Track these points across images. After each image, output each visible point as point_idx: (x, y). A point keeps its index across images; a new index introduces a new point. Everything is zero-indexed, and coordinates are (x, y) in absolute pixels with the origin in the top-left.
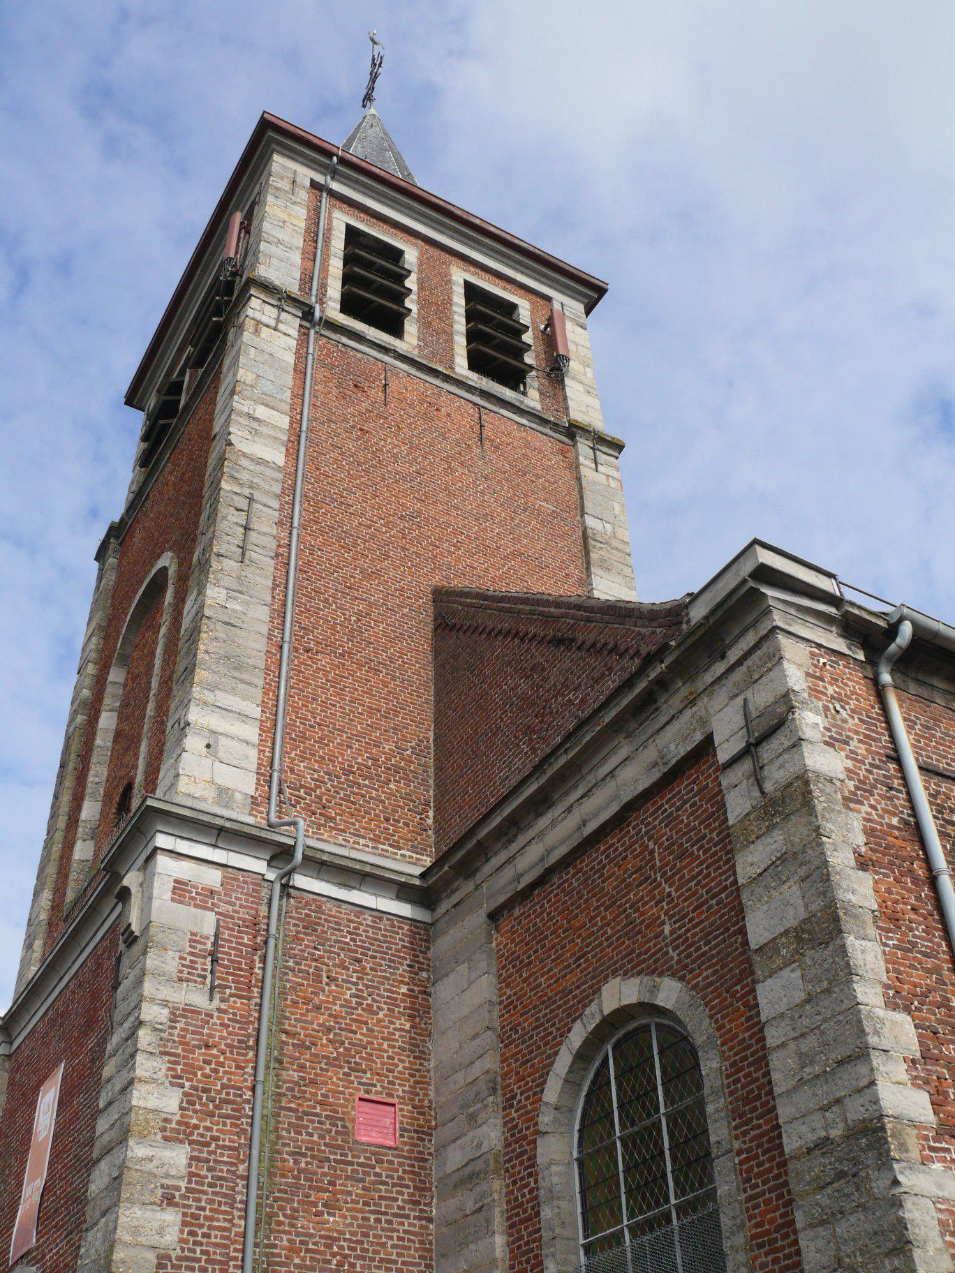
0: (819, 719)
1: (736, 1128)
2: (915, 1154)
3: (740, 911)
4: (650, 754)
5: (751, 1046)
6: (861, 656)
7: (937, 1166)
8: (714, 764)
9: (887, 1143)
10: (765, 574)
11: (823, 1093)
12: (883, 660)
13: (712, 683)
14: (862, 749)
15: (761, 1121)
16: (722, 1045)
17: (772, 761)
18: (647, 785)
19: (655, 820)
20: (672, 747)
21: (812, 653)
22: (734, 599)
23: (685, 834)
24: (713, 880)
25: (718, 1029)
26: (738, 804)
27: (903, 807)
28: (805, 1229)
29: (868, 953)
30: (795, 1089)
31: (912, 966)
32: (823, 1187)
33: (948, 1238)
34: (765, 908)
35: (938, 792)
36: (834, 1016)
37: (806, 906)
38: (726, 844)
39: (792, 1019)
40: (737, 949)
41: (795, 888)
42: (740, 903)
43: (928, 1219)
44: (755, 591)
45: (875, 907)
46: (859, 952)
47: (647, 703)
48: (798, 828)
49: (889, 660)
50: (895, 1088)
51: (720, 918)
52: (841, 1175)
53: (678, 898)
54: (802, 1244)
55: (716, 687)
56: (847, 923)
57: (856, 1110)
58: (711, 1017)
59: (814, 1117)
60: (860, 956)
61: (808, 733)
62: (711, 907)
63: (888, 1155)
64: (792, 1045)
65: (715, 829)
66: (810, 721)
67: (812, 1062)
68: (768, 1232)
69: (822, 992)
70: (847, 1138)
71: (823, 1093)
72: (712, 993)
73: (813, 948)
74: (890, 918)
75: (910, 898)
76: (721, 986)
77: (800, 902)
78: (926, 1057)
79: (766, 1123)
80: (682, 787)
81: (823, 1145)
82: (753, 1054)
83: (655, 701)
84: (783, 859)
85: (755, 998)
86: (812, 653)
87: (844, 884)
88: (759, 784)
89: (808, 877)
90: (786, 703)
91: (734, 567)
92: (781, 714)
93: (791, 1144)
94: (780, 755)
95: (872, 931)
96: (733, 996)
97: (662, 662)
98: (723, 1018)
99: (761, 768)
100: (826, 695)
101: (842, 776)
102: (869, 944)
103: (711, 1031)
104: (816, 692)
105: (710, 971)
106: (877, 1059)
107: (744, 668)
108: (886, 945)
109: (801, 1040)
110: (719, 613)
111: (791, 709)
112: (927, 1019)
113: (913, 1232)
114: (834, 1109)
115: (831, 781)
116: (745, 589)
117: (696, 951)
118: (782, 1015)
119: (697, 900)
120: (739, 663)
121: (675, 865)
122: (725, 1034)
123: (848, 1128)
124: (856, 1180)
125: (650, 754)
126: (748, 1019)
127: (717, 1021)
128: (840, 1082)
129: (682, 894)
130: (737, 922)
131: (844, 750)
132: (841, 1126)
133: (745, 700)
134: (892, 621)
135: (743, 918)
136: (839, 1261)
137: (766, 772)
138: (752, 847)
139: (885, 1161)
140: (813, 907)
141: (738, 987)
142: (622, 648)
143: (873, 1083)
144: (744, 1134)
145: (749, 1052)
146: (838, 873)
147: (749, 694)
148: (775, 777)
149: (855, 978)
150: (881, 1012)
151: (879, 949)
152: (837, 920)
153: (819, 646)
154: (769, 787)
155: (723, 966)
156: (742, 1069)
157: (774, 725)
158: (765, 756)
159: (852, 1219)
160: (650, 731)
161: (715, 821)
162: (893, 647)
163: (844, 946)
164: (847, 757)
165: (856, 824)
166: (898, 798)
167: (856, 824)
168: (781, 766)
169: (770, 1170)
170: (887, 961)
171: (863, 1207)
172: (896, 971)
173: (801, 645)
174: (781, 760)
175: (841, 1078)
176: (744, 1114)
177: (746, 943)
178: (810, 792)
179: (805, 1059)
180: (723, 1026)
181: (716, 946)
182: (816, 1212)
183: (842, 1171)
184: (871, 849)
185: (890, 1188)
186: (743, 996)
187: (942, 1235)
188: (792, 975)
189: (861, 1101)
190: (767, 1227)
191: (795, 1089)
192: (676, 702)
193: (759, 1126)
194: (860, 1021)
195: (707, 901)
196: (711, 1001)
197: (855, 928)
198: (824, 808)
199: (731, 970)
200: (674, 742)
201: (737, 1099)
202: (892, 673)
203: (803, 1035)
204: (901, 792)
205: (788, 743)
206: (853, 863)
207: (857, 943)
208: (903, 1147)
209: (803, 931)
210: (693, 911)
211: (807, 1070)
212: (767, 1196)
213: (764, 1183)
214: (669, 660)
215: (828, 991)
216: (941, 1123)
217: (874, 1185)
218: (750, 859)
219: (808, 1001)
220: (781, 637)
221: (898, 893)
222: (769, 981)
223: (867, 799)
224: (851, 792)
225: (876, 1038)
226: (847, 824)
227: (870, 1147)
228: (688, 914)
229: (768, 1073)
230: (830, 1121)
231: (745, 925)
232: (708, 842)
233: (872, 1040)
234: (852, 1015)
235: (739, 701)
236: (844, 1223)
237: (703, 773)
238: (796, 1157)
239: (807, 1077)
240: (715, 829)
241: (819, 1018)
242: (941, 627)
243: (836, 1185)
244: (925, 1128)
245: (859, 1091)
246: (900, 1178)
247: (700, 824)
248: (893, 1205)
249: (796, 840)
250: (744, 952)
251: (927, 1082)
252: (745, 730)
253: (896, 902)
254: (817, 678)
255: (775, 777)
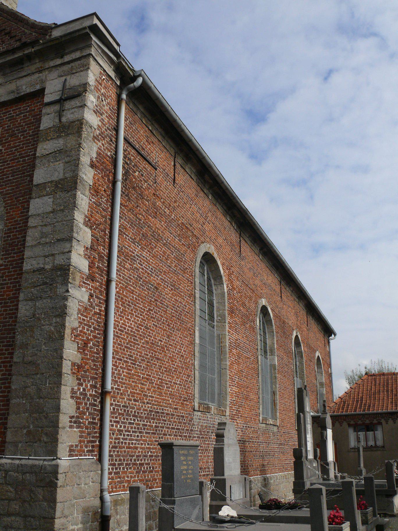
0: (94, 100)
1: (3, 255)
2: (77, 283)
3: (33, 167)
4: (12, 87)
5: (20, 224)
6: (118, 83)
7: (84, 289)
8: (40, 102)
9: (69, 275)
10: (94, 29)
11: (47, 250)
12: (126, 89)
13: (53, 67)
14: (106, 120)
15: (15, 255)
16: (7, 220)
17: (69, 109)
18: (5, 100)
19: (4, 116)
20: (24, 87)
21: (101, 72)
22: (77, 34)
23: (17, 127)
24: (23, 150)
25: (7, 213)
26: (47, 122)
27: (113, 150)
28: (23, 301)
29: (83, 201)
30: (35, 246)
31: (97, 212)
32: (36, 287)
33: (79, 316)
34: (46, 169)
35: (127, 150)
36: (62, 221)
37: (64, 173)
38: (37, 136)
39: (43, 217)
40: (26, 182)
41: (62, 165)
42: (35, 164)
43: (75, 307)
44: (88, 35)
45: (91, 184)
46: (80, 199)
47: (18, 64)
48: (71, 141)
49: (128, 90)
50: (78, 256)
51: (22, 167)
52: (45, 283)
53: (5, 153)
54: (20, 306)
55: (54, 69)
56: (80, 186)
57: (59, 260)
58: (5, 207)
59: (40, 259)
60: (80, 201)
61: (89, 104)
62: (20, 161)
63: (68, 280)
64: (40, 228)
65: (32, 129)
66: (91, 99)
67: (46, 237)
68: (5, 299)
69: (60, 210)
70: (52, 270)
71: (47, 250)
72: (8, 197)
73: (61, 192)
74: (95, 191)
75: (105, 186)
76: (14, 195)
77: (62, 171)
78: (92, 248)
79: (17, 256)
80: (22, 106)
81: (41, 270)
82: (19, 227)
83: (23, 64)
84: (60, 151)
85: (29, 205)
86: (101, 72)
87: (83, 170)
88: (60, 117)
89: (68, 162)
90: (84, 88)
91: (81, 21)
92: (80, 91)
93: (26, 267)
94: (74, 108)
95: (87, 193)
96: (18, 201)
97: (33, 48)
98: (10, 209)
99: (63, 111)
100: (100, 92)
101: (96, 127)
102: (85, 198)
103: (3, 213)
104: (97, 89)
105: (10, 188)
106: (74, 243)
107: (70, 66)
108: (91, 200)
109: (45, 227)
110: (68, 37)
111: (85, 91)
112: (96, 234)
113: (69, 311)
114: (50, 258)
115: (91, 127)
116: (84, 32)
117: (6, 178)
118: (39, 215)
119: (13, 157)
120: (69, 63)
121: (8, 139)
122: (10, 216)
123: (54, 266)
124: (51, 287)
125: (12, 87)
126: (21, 213)
127: (7, 210)
128: (56, 248)
129: (7, 152)
130: (29, 171)
131: (100, 117)
132: (51, 265)
133: (66, 80)
134: (135, 75)
135: (33, 171)
136: (34, 315)
137: (64, 113)
138: (47, 142)
139: (65, 282)
140: (67, 175)
141: (21, 198)
142: (13, 35)
143: (70, 251)
144: (6, 258)
145: (18, 226)
146: (82, 165)
147: (68, 78)
148: (68, 116)
149: (76, 209)
150: (81, 226)
151: (88, 201)
152: (76, 183)
153: (105, 71)
154: (64, 119)
155: (16, 188)
156: (13, 232)
157: (75, 94)
158: (67, 106)
159: (44, 301)
160: (16, 77)
161: (33, 126)
162: (132, 85)
163: (75, 195)
164: (100, 121)
165: (95, 148)
166: (112, 146)
167: (95, 148)
168: (72, 113)
169: (13, 275)
170: (89, 207)
171: (51, 297)
172: (91, 212)
173: (98, 67)
174: (73, 110)
175: (57, 246)
176: (8, 250)
177: (32, 181)
178: (82, 128)
179: (43, 235)
180: (9, 212)
181: (16, 179)
182: (30, 295)
183: (46, 282)
184: (97, 161)
185: (64, 293)
186: (23, 202)
187: (78, 314)
188: (49, 200)
189: (63, 257)
190: (5, 297)
191: (35, 246)
192: (33, 68)
193: (14, 257)
194: (72, 226)
195: (18, 158)
196: (7, 200)
197: (82, 189)
198: (85, 137)
199: (21, 190)
200: (26, 85)
201: (7, 244)
202: (127, 95)
203: (46, 225)
204: (114, 144)
205: (79, 104)
206: (89, 163)
207: (81, 195)
208: (74, 279)
209: (59, 183)
210: (10, 161)
211: (43, 239)
212: (9, 285)
213: (9, 280)
214: (36, 48)
215: (62, 211)
216: (90, 274)
217: (58, 290)
218: (45, 147)
219: (52, 212)
220: (91, 59)
221: (101, 182)
222: (37, 200)
223: (102, 141)
224: (97, 135)
225: (77, 235)
226: (91, 147)
227: (61, 275)
228: (8, 161)
229: (25, 237)
230: (47, 262)
231: (33, 174)
232: (27, 134)
233: (75, 235)
234: (70, 224)
235: (63, 79)
236: (40, 302)
237: (34, 104)
238: (27, 273)
239: (42, 242)
240: (32, 129)
241: (55, 220)
242: (153, 86)
243: (41, 287)
244: (84, 274)
245: (64, 253)
246: (70, 290)
247: (25, 125)
248: (63, 299)
249: (69, 145)
250: (29, 185)
251: (89, 258)
252: (61, 92)
253: (100, 185)
254: (99, 83)
255: (68, 116)
